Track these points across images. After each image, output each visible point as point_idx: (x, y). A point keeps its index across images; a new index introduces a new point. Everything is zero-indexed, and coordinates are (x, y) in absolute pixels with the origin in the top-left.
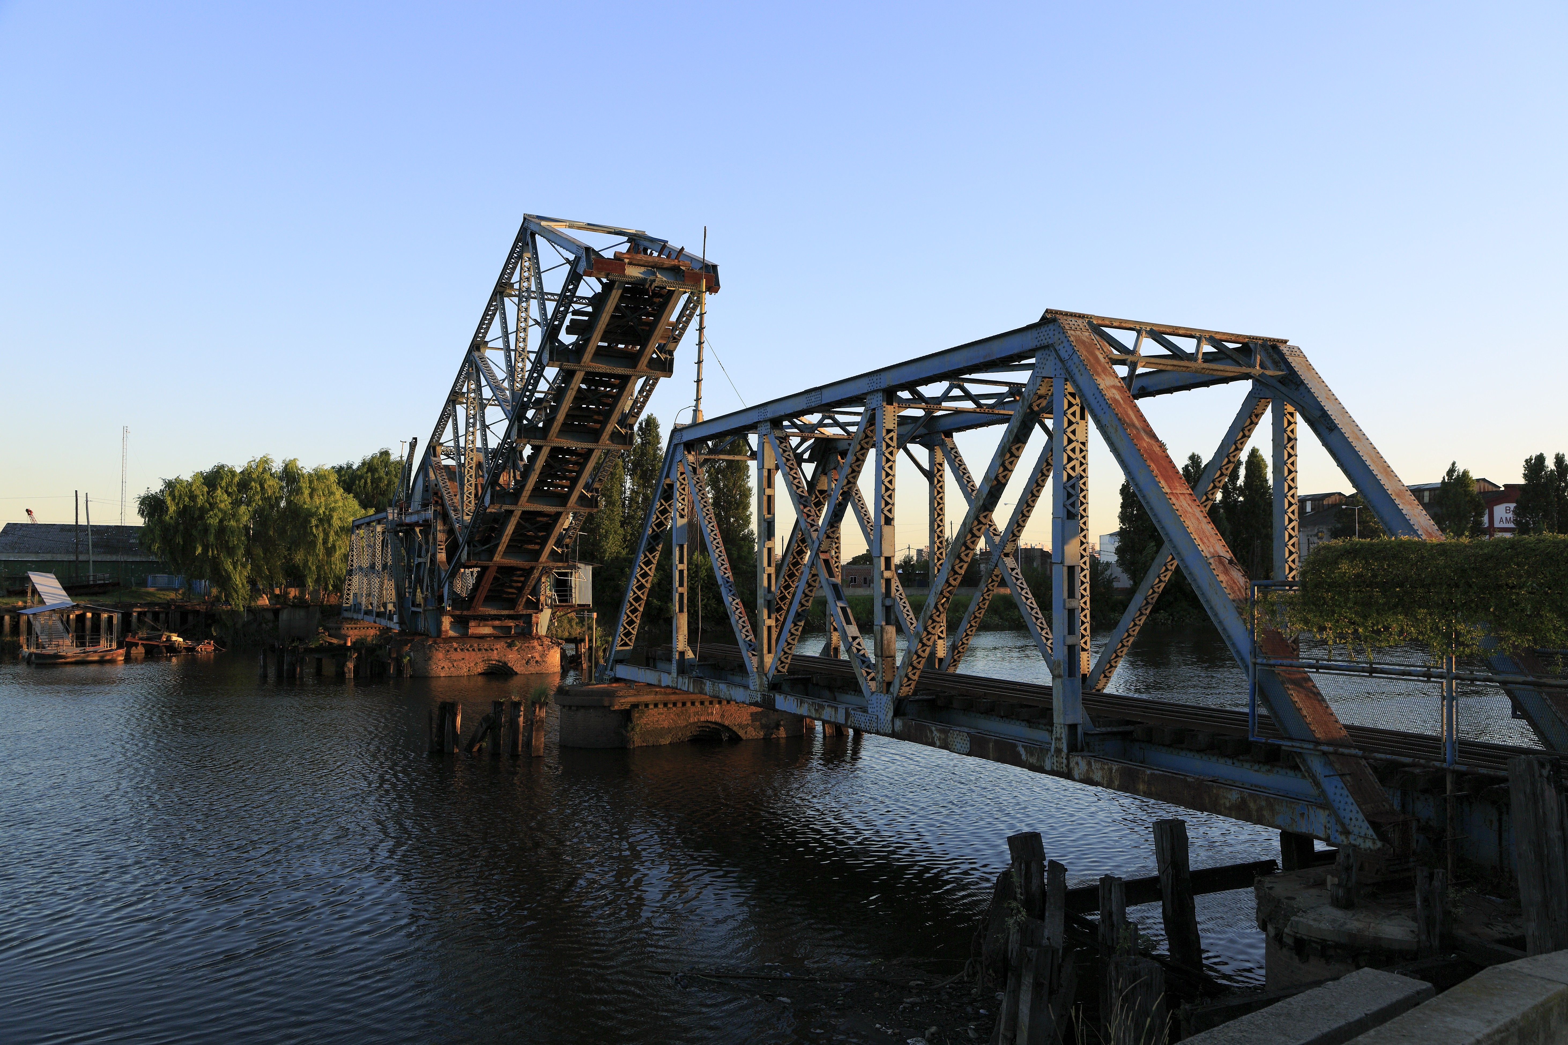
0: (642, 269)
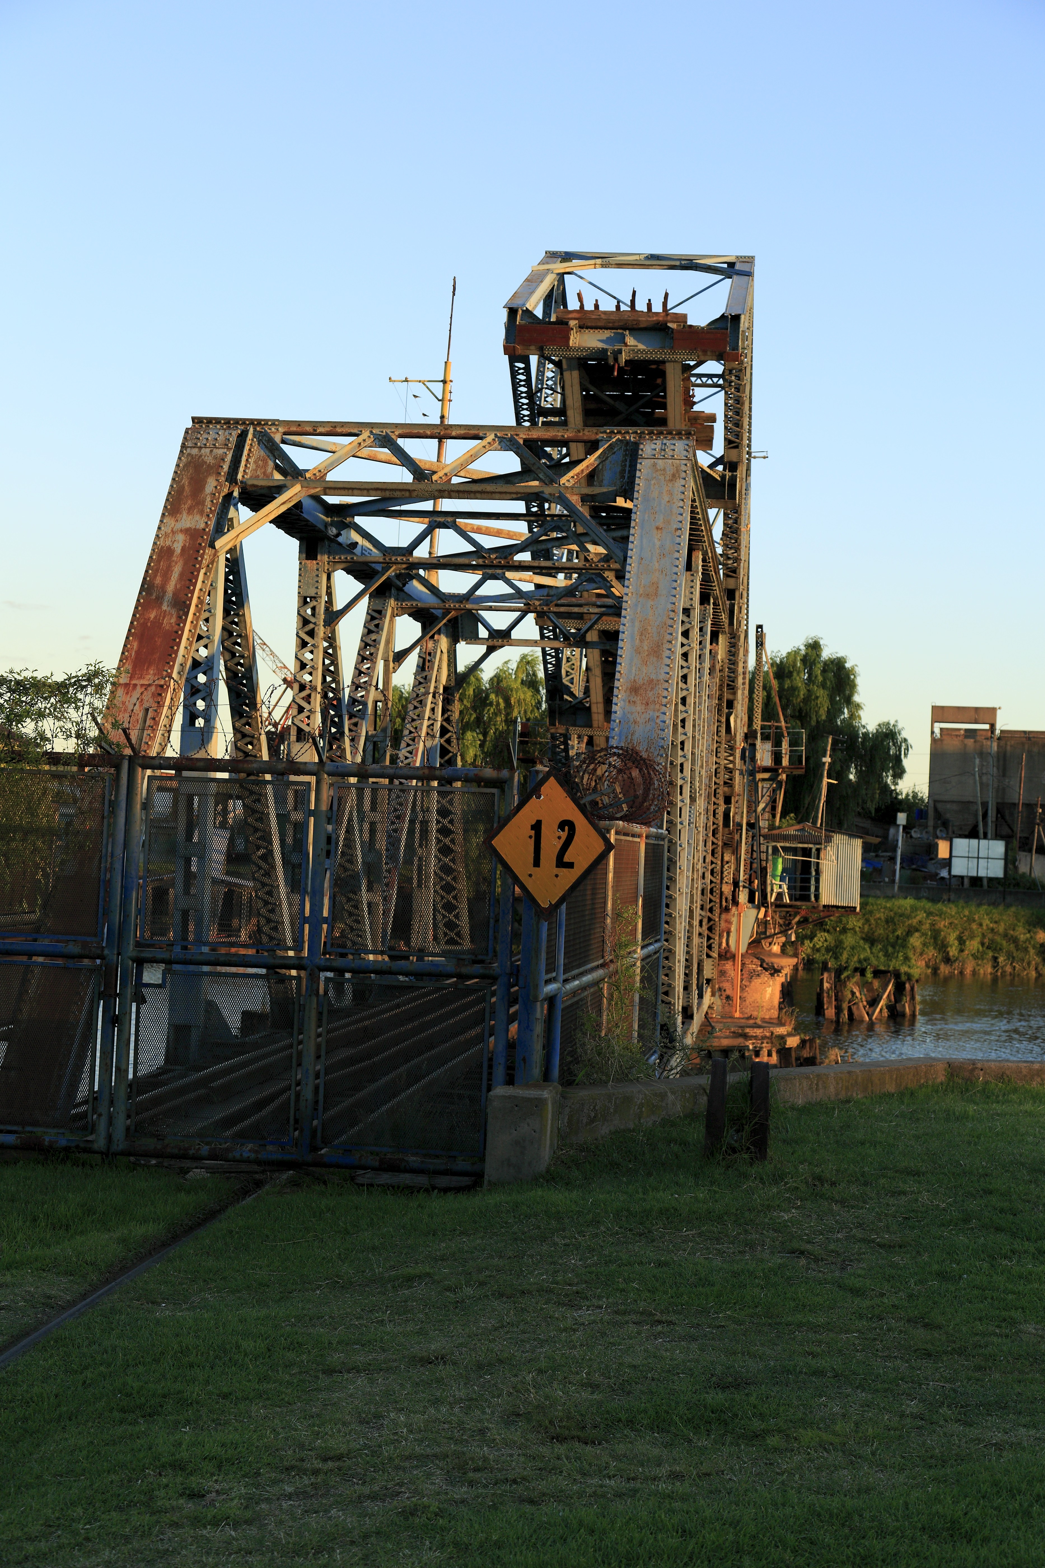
0: (607, 334)
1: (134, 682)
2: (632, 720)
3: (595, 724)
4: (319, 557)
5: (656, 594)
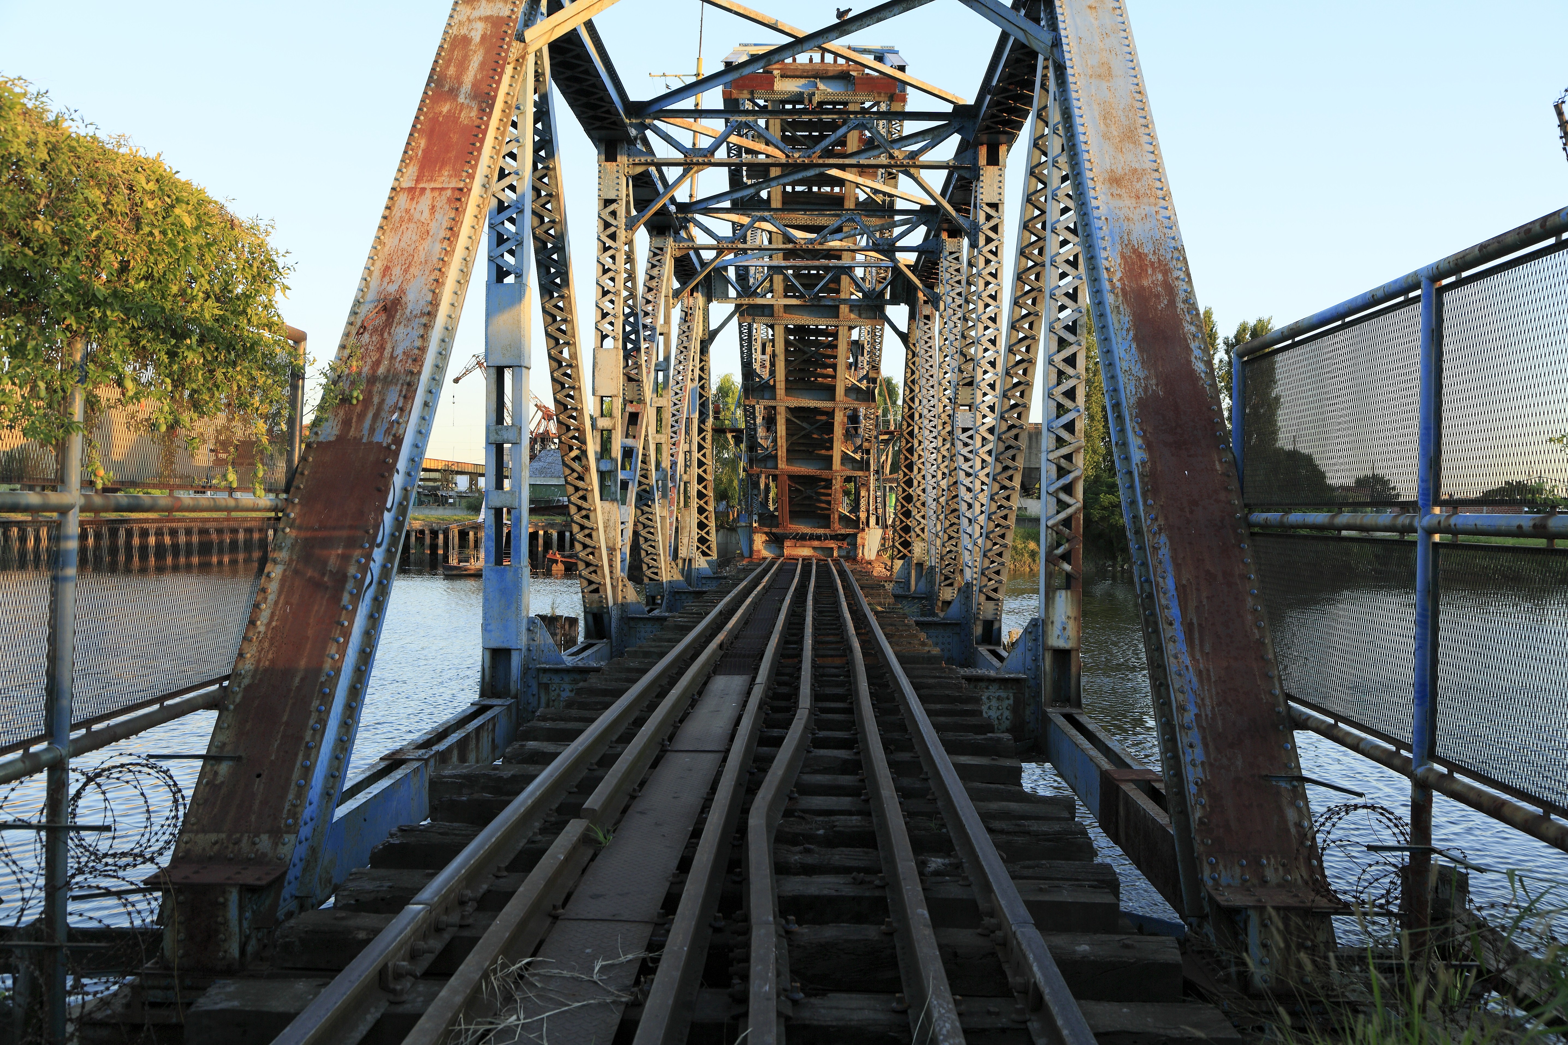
0: (803, 81)
1: (421, 185)
2: (1122, 216)
3: (778, 397)
4: (619, 158)
5: (1110, 75)
